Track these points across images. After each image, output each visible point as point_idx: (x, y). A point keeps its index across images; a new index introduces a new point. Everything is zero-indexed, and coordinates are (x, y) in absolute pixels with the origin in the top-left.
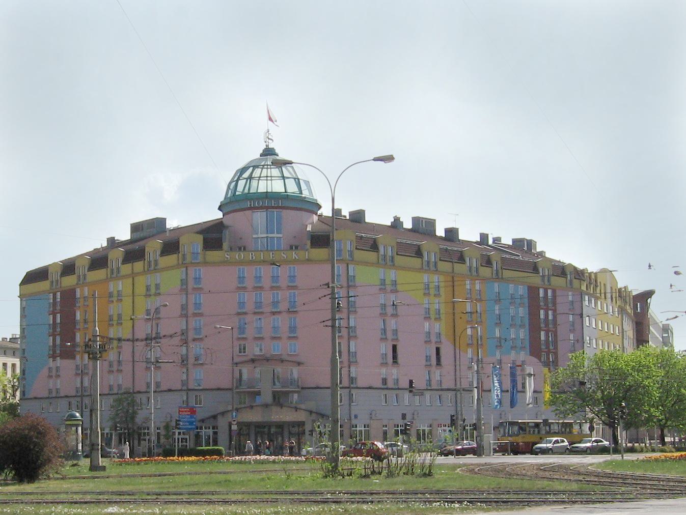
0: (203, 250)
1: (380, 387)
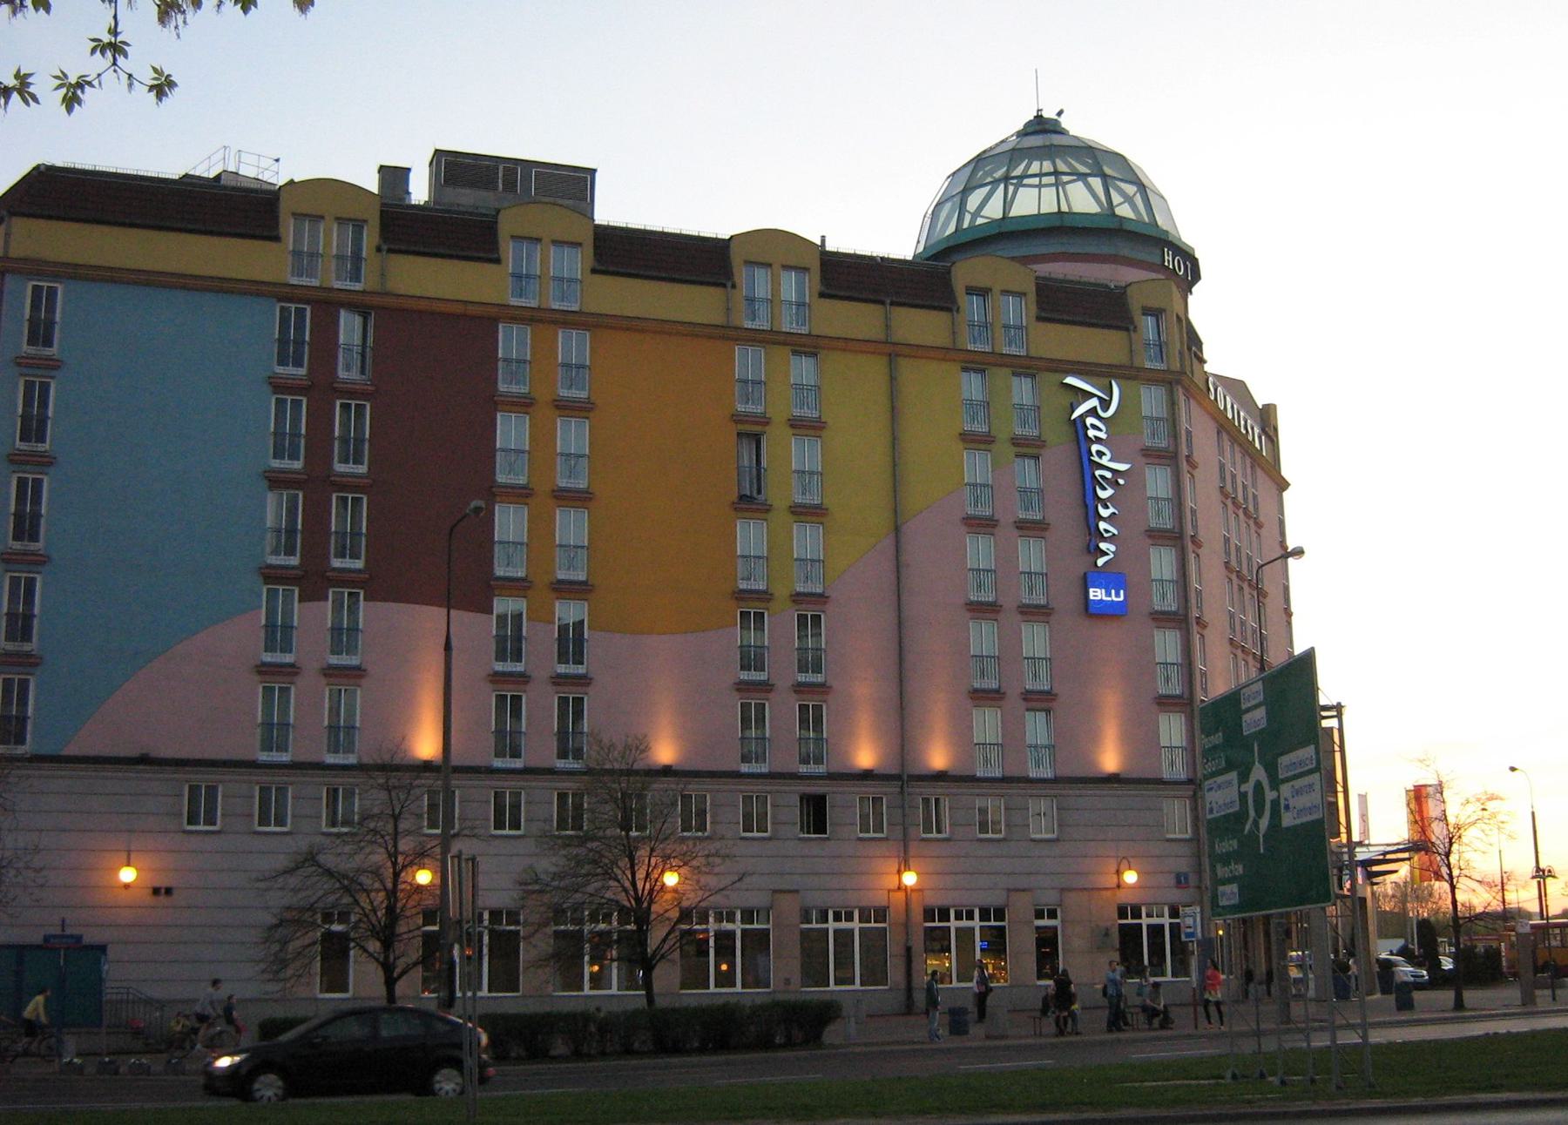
0: (379, 250)
1: (545, 764)
